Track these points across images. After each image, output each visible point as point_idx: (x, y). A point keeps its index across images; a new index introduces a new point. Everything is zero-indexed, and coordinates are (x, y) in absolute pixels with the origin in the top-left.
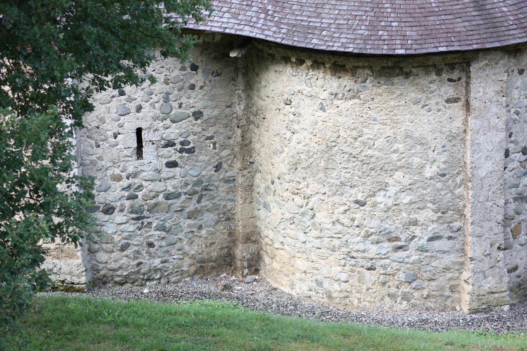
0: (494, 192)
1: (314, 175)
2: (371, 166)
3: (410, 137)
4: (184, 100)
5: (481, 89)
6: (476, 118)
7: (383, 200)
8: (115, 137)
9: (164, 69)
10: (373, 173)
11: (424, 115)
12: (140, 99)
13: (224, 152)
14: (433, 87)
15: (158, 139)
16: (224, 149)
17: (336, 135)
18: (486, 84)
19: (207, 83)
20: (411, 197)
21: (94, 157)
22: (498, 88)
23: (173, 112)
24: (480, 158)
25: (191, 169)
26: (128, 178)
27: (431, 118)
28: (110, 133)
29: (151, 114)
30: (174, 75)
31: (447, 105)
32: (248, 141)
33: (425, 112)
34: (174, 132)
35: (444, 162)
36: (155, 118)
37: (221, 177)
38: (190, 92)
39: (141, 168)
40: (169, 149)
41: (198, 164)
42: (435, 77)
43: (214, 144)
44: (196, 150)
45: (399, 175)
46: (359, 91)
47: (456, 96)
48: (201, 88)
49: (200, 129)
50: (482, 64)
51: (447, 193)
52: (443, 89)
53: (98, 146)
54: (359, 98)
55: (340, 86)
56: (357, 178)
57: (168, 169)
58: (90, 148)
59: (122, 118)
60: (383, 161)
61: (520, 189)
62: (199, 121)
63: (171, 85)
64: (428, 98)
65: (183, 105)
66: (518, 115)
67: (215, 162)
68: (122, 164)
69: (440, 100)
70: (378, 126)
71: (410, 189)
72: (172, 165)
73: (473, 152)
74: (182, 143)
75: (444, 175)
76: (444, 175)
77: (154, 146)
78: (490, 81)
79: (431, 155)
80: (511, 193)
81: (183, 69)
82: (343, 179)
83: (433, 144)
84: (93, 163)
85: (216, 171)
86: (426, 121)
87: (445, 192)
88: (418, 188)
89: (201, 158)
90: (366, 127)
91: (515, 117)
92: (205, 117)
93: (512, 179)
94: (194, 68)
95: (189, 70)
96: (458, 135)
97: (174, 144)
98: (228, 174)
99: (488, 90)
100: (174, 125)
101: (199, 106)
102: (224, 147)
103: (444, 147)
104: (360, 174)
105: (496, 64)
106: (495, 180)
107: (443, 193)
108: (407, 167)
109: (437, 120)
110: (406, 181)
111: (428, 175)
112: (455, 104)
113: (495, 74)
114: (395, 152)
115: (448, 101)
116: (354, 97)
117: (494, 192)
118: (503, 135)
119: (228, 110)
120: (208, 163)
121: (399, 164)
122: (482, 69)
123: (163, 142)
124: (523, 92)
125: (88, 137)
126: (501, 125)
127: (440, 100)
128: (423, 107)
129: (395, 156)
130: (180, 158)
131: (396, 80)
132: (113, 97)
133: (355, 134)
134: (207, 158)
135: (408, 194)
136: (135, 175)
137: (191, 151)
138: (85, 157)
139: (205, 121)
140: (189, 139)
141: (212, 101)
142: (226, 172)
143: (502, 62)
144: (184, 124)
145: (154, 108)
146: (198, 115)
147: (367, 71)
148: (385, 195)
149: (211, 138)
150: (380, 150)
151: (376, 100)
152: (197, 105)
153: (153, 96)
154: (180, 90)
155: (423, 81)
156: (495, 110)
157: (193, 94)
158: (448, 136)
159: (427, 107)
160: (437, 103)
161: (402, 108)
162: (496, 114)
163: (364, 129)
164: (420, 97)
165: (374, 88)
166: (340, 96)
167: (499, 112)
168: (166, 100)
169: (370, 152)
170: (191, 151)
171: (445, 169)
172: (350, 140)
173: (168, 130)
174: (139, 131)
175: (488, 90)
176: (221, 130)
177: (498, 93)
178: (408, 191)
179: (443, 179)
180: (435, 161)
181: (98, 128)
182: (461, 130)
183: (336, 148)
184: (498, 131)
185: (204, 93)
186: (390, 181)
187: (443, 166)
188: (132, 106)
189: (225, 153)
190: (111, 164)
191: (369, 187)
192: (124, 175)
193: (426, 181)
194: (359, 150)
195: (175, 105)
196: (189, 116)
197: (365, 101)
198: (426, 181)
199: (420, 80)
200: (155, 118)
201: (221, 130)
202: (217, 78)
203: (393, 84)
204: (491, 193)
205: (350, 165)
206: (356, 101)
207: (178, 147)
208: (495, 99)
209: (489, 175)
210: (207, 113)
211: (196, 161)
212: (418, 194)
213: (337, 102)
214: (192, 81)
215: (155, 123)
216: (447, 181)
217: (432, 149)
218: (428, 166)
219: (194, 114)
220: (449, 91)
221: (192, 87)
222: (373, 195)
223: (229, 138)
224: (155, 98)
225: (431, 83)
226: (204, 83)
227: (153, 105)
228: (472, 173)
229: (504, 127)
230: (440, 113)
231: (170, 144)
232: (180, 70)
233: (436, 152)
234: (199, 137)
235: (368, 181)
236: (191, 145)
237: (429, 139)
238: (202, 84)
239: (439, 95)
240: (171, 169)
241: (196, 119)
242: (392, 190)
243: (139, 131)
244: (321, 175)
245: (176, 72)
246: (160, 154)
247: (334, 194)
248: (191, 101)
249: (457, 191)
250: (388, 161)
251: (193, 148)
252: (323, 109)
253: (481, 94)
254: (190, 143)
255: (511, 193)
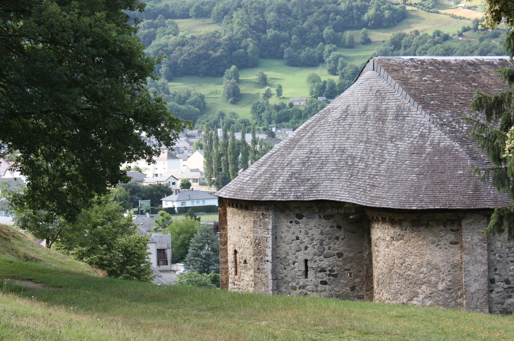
0: (481, 303)
1: (385, 288)
2: (410, 281)
3: (430, 264)
4: (332, 245)
5: (469, 237)
6: (467, 254)
7: (416, 303)
8: (294, 264)
9: (321, 226)
10: (411, 286)
11: (437, 251)
12: (306, 242)
13: (357, 279)
14: (442, 234)
15: (316, 267)
16: (357, 278)
17: (393, 262)
18: (473, 236)
19: (347, 237)
20: (431, 302)
21: (283, 275)
22: (481, 237)
23: (325, 252)
24: (470, 280)
25: (335, 287)
26: (300, 289)
27: (441, 253)
28: (291, 261)
29: (313, 252)
30: (326, 230)
31: (451, 246)
32: (370, 274)
33: (438, 249)
34: (325, 263)
35: (450, 281)
36: (315, 254)
37: (355, 295)
38: (336, 241)
39: (307, 283)
40: (323, 273)
41: (340, 284)
42: (442, 228)
43: (350, 274)
44: (339, 276)
45: (424, 287)
46: (403, 236)
47: (456, 241)
48: (343, 239)
49: (341, 264)
50: (469, 221)
51: (452, 301)
52: (448, 236)
53: (285, 269)
54: (403, 239)
55: (395, 232)
56: (403, 289)
57: (321, 285)
58: (281, 270)
59: (297, 253)
60: (416, 279)
61: (505, 306)
62: (341, 259)
63: (324, 235)
64: (439, 241)
65: (331, 248)
66: (501, 258)
67: (351, 284)
68: (297, 280)
69: (446, 242)
70: (413, 257)
71: (430, 297)
72: (324, 283)
73: (466, 275)
74: (330, 271)
75: (450, 289)
76: (450, 289)
77: (314, 271)
78: (475, 232)
79: (442, 275)
80: (497, 308)
81: (332, 227)
82: (397, 290)
83: (443, 269)
84: (282, 278)
85: (351, 291)
86: (438, 254)
87: (451, 300)
88: (434, 296)
89: (341, 281)
90: (407, 257)
91: (499, 259)
92: (344, 257)
93: (497, 298)
94: (339, 227)
95: (335, 228)
96: (458, 265)
97: (325, 271)
98: (359, 294)
99: (474, 238)
100: (326, 259)
101: (341, 249)
102: (357, 276)
103: (449, 271)
104: (404, 286)
105: (479, 222)
106: (482, 296)
107: (449, 300)
108: (429, 282)
109: (445, 254)
110: (428, 292)
111: (440, 288)
112: (456, 246)
113: (478, 228)
114: (421, 273)
115: (451, 243)
116: (401, 239)
117: (481, 303)
118: (486, 267)
119: (359, 255)
120: (346, 285)
121: (424, 280)
122: (470, 224)
123: (319, 269)
124: (504, 244)
125: (281, 263)
126: (484, 260)
127: (446, 242)
128: (437, 246)
129: (422, 276)
130: (329, 279)
131: (421, 229)
132: (293, 240)
133: (401, 261)
134: (345, 282)
135: (429, 300)
136: (303, 287)
137: (335, 276)
138: (279, 275)
139: (344, 259)
140: (334, 269)
141: (349, 248)
142: (359, 292)
143: (483, 221)
144: (331, 259)
145: (314, 248)
146: (340, 255)
147: (407, 223)
148: (417, 300)
149: (349, 270)
150: (414, 272)
151: (412, 241)
152: (339, 249)
153: (314, 241)
154: (329, 239)
155: (436, 230)
156: (479, 250)
157: (338, 243)
158: (452, 265)
159: (439, 246)
160: (445, 244)
161: (425, 246)
162: (481, 253)
163: (406, 259)
164: (435, 239)
165: (411, 233)
166: (395, 238)
167: (482, 252)
168: (321, 244)
169: (409, 273)
170: (335, 276)
171: (450, 286)
172: (399, 265)
173: (322, 262)
174: (306, 261)
175: (474, 238)
176: (355, 266)
177: (481, 240)
178: (429, 298)
179: (449, 291)
180: (444, 280)
181: (285, 258)
182: (460, 262)
183: (393, 270)
184: (482, 264)
185: (344, 242)
186: (420, 291)
187: (449, 284)
188: (302, 246)
189: (357, 280)
190: (291, 280)
191: (409, 295)
192: (298, 286)
193: (439, 292)
194: (404, 271)
195: (326, 247)
196: (335, 255)
197: (407, 241)
198: (439, 292)
199: (434, 229)
200: (315, 254)
201: (355, 266)
202: (352, 235)
203: (419, 231)
204: (478, 303)
205: (400, 281)
206: (402, 241)
207: (328, 272)
208: (479, 244)
209: (477, 292)
210: (345, 254)
211: (339, 282)
212: (435, 300)
213: (394, 242)
214: (337, 235)
215: (315, 257)
216: (452, 293)
217: (442, 272)
218: (440, 283)
219: (338, 254)
220: (451, 237)
221: (337, 238)
222: (411, 300)
223: (360, 272)
224: (315, 243)
225: (440, 231)
226: (345, 237)
227: (313, 246)
228: (465, 289)
229: (486, 262)
230: (446, 250)
231: (323, 270)
232: (330, 227)
233: (444, 274)
234: (341, 269)
235: (408, 290)
236: (336, 273)
237: (440, 266)
238: (343, 237)
239: (446, 239)
240: (323, 286)
241: (339, 257)
242: (421, 297)
243: (306, 261)
244: (387, 288)
245: (328, 229)
246: (317, 276)
247: (393, 300)
248: (336, 246)
249: (459, 301)
250: (418, 278)
251: (337, 274)
252: (387, 247)
253: (469, 240)
254: (335, 271)
255: (497, 308)
